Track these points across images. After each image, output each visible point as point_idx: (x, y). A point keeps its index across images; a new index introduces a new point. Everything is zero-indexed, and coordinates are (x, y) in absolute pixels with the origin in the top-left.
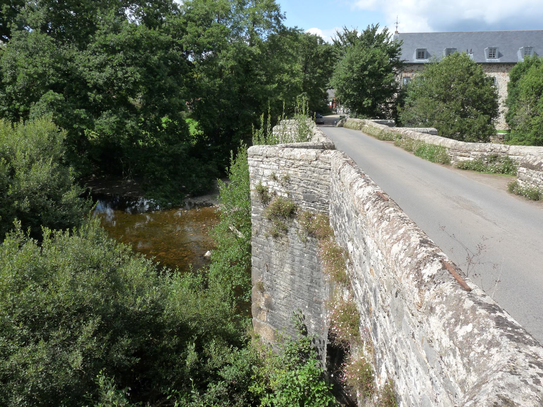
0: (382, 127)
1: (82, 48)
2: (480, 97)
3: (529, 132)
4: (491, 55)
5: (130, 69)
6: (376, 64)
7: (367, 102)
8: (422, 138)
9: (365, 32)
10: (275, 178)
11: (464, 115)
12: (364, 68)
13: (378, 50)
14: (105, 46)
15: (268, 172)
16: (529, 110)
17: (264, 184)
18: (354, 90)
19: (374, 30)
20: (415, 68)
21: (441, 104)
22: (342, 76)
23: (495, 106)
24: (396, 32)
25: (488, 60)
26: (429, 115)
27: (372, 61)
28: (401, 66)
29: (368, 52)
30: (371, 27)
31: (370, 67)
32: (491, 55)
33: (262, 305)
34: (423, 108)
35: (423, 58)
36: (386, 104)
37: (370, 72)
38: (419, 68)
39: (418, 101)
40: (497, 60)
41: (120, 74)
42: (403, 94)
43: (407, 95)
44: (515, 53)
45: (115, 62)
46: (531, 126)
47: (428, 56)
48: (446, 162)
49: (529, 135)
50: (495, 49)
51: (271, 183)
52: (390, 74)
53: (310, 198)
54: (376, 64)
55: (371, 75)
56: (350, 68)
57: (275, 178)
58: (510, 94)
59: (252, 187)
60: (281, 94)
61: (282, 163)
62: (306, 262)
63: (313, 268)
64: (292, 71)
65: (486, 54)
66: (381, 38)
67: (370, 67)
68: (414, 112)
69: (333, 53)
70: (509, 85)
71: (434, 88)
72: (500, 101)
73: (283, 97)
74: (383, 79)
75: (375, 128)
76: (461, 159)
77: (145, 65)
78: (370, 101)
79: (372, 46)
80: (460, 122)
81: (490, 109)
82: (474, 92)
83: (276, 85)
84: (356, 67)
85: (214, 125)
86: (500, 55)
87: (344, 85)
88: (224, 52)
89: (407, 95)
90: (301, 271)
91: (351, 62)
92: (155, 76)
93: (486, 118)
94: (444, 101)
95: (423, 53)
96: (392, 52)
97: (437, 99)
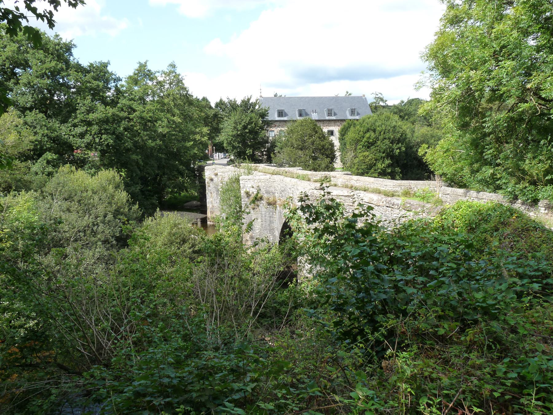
0: (274, 168)
1: (64, 122)
2: (323, 146)
3: (354, 168)
4: (329, 114)
5: (104, 136)
6: (253, 125)
7: (249, 151)
8: (297, 172)
9: (243, 101)
10: (253, 187)
11: (315, 159)
12: (245, 127)
13: (253, 115)
14: (85, 121)
15: (250, 185)
16: (353, 154)
17: (248, 190)
18: (239, 143)
19: (249, 100)
20: (277, 124)
21: (300, 152)
22: (231, 133)
23: (332, 151)
24: (261, 96)
25: (327, 118)
26: (293, 159)
27: (250, 123)
28: (270, 124)
29: (246, 116)
30: (247, 98)
31: (249, 126)
32: (329, 114)
33: (248, 238)
34: (289, 154)
35: (282, 116)
36: (262, 152)
37: (249, 130)
38: (280, 124)
39: (285, 150)
40: (334, 118)
41: (97, 140)
42: (273, 145)
43: (276, 146)
44: (345, 112)
45: (93, 132)
46: (354, 164)
47: (286, 115)
48: (309, 180)
49: (354, 170)
50: (331, 110)
51: (251, 189)
52: (263, 132)
53: (268, 192)
54: (253, 125)
55: (250, 132)
56: (235, 128)
57: (253, 187)
58: (341, 144)
59: (242, 192)
60: (196, 149)
61: (256, 181)
62: (268, 215)
63: (270, 217)
64: (202, 133)
65: (326, 113)
66: (254, 105)
67: (249, 126)
68: (282, 157)
69: (220, 116)
70: (339, 139)
71: (294, 141)
72: (335, 148)
73: (198, 150)
74: (258, 135)
75: (269, 169)
76: (315, 178)
77: (114, 133)
78: (251, 151)
79: (249, 112)
80: (313, 163)
81: (330, 154)
82: (319, 144)
83: (192, 143)
84: (239, 127)
85: (154, 172)
86: (335, 114)
87: (232, 139)
88: (159, 122)
89: (276, 146)
90: (266, 219)
91: (235, 123)
92: (121, 141)
93: (328, 160)
94: (301, 149)
95: (282, 113)
96: (263, 115)
97: (297, 148)
